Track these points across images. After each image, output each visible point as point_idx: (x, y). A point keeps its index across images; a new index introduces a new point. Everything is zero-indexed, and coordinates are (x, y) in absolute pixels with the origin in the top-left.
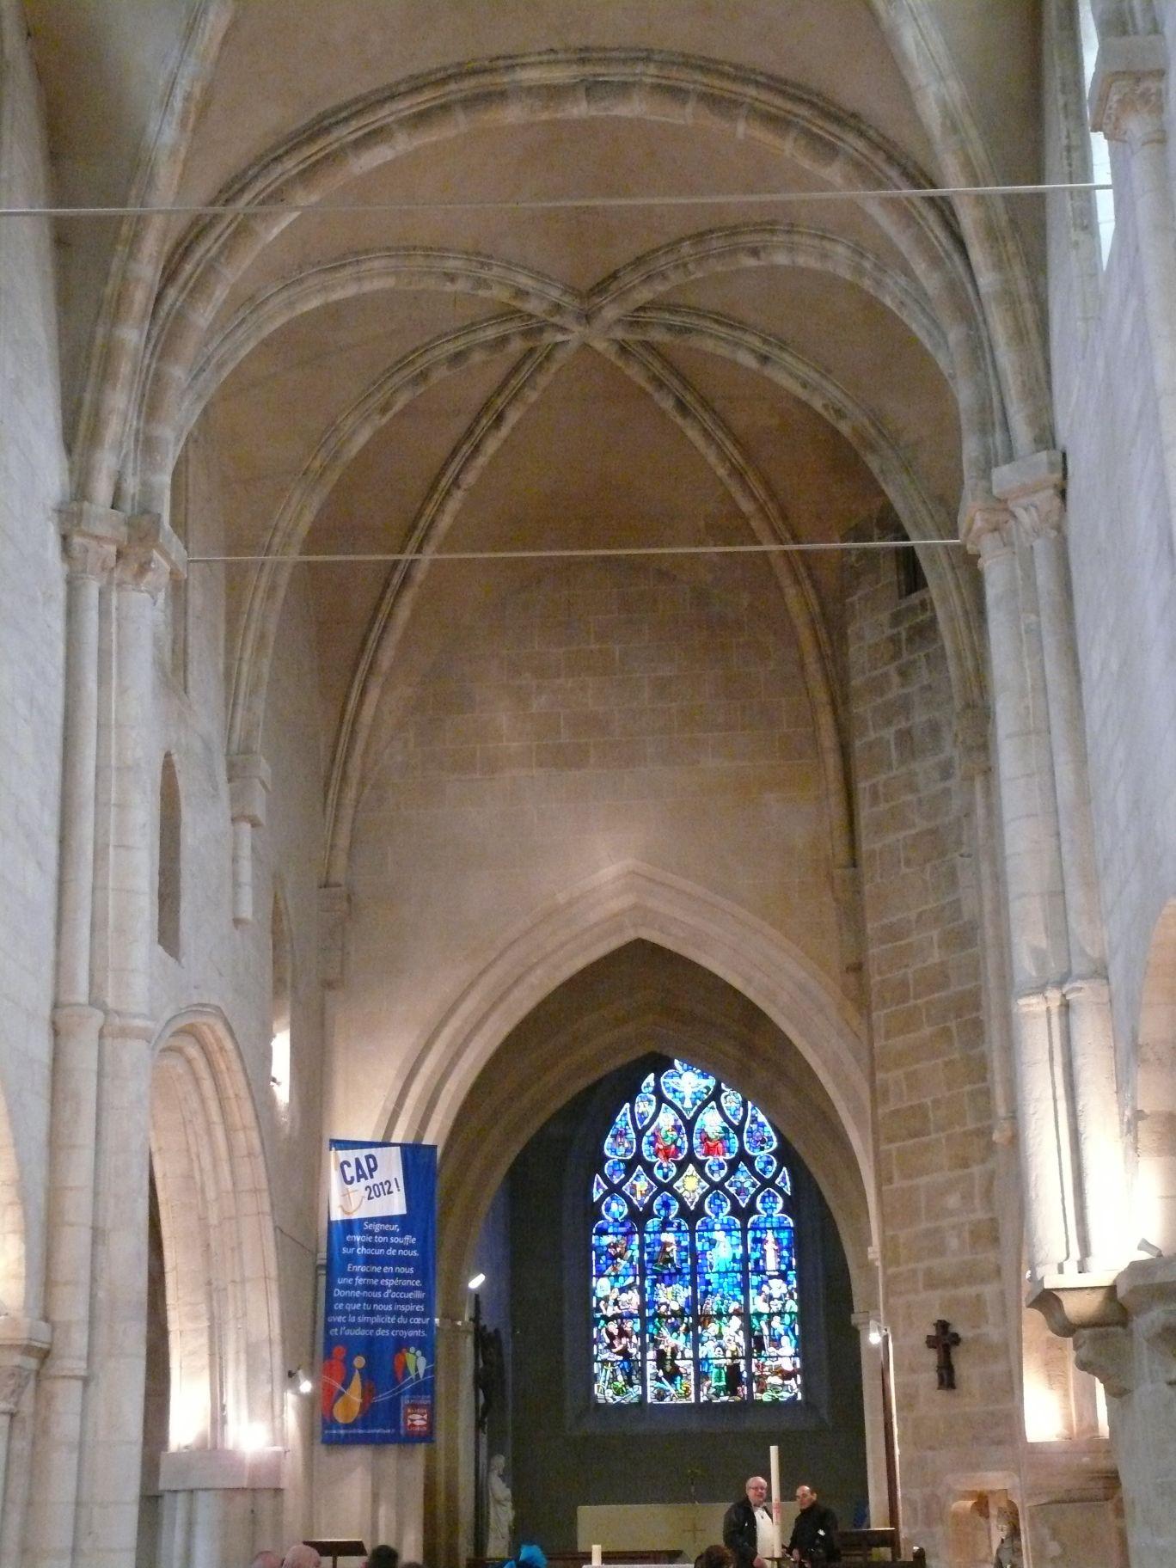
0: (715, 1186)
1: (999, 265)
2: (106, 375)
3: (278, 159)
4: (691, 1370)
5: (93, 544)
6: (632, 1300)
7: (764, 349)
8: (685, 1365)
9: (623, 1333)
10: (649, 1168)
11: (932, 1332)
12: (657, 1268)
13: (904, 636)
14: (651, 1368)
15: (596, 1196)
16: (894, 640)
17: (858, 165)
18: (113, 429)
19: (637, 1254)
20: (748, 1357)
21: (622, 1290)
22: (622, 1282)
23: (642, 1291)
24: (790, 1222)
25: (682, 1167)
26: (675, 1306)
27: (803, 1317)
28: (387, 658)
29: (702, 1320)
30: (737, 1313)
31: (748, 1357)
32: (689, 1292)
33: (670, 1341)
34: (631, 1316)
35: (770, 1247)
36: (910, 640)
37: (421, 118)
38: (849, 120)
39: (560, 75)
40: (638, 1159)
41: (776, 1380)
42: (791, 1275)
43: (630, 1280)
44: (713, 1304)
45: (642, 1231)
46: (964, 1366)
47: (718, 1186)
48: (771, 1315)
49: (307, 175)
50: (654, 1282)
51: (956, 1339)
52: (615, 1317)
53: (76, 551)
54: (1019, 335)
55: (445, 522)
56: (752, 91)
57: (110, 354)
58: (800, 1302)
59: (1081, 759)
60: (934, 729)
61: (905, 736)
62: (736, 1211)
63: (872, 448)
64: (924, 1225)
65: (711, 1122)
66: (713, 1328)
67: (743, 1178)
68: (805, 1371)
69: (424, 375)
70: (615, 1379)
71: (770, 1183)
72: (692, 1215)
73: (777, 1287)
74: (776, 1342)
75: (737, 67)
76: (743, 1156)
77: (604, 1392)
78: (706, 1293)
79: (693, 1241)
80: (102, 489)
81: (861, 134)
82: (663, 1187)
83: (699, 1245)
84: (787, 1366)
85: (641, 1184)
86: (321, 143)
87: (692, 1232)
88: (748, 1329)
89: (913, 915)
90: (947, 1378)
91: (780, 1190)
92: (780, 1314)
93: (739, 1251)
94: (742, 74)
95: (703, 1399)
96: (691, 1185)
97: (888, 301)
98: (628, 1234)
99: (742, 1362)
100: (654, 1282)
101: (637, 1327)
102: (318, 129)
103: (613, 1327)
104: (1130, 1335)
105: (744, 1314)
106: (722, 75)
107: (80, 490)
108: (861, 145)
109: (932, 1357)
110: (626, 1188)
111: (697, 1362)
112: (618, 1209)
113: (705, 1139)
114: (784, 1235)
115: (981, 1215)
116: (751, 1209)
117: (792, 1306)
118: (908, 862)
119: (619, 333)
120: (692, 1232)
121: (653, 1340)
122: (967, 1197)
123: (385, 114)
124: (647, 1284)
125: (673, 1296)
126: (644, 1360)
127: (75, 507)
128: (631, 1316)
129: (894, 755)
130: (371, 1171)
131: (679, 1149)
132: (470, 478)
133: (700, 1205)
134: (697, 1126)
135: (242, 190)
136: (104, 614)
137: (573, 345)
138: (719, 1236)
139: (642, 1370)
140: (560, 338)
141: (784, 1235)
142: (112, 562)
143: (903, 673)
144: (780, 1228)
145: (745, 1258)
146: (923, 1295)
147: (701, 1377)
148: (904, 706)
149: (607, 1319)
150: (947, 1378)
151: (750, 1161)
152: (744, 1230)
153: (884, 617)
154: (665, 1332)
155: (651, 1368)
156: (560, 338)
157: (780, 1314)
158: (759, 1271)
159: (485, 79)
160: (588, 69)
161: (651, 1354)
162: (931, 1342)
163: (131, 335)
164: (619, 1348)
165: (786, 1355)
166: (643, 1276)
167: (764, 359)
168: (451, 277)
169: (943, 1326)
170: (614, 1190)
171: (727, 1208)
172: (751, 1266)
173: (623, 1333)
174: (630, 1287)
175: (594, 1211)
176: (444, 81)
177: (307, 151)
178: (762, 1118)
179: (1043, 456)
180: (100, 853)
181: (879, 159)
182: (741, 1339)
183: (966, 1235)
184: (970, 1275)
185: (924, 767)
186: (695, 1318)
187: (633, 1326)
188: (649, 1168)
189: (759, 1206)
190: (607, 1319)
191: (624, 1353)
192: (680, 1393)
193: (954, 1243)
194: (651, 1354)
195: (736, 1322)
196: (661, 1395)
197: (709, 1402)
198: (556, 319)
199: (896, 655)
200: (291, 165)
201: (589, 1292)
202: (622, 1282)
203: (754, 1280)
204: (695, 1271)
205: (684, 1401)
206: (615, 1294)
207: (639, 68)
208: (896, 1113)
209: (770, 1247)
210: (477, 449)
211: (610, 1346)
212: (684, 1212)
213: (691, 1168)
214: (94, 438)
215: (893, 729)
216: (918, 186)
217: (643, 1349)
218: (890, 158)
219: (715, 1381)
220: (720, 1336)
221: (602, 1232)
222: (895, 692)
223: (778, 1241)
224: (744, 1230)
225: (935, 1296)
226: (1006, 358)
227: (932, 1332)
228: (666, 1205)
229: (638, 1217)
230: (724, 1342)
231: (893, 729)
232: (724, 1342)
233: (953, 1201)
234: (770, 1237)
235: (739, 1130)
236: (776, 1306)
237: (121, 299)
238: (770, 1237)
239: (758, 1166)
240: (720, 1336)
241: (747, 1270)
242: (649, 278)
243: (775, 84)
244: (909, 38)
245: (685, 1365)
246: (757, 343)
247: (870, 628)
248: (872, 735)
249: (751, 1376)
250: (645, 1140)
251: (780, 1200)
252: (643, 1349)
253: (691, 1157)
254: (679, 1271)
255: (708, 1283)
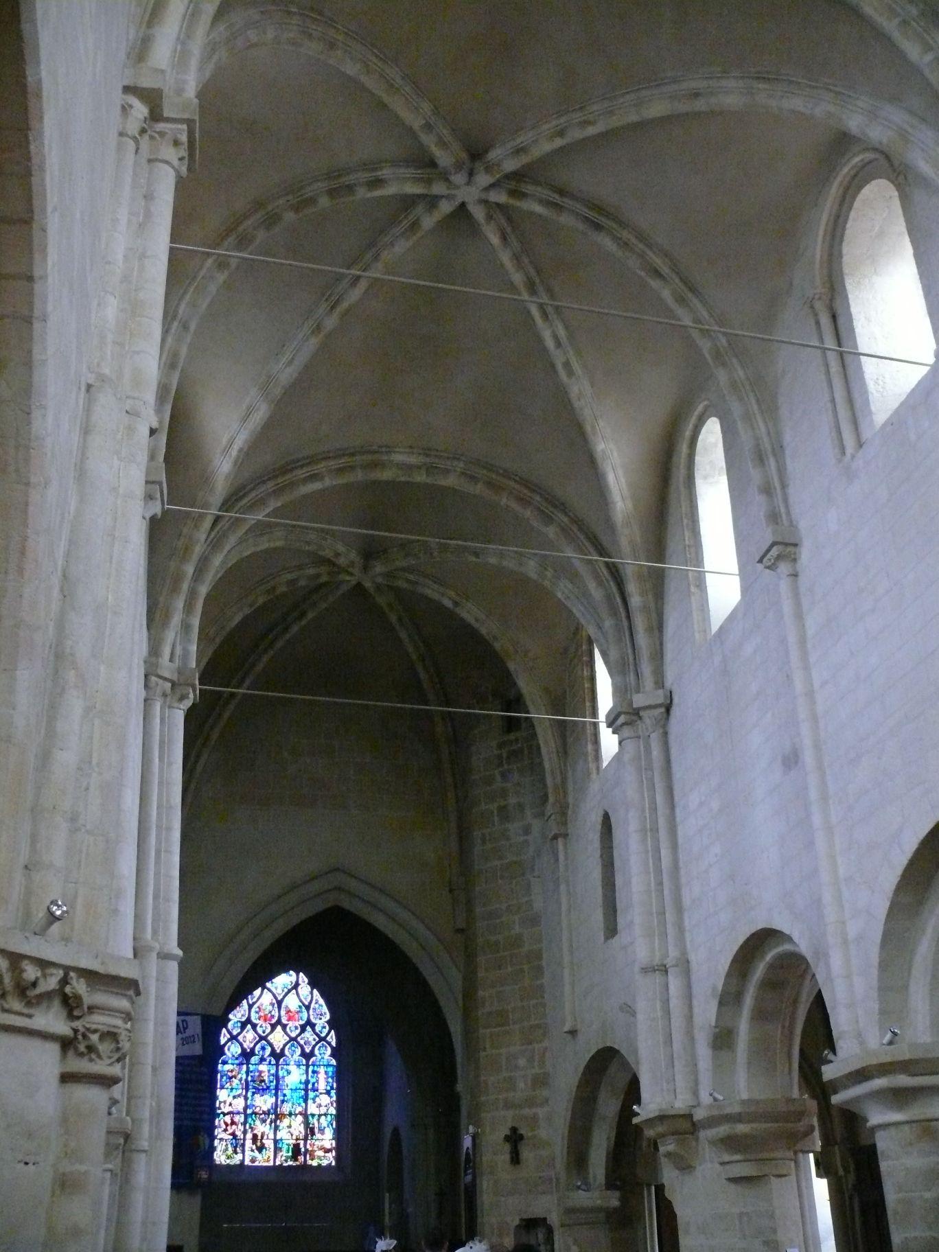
0: (292, 1039)
1: (643, 593)
2: (175, 589)
3: (264, 482)
4: (272, 1146)
5: (161, 681)
6: (239, 1104)
7: (458, 599)
8: (269, 1144)
9: (233, 1123)
10: (254, 1026)
11: (508, 1133)
12: (256, 1086)
13: (505, 755)
14: (249, 1143)
15: (223, 1041)
16: (500, 757)
17: (563, 529)
18: (176, 619)
19: (244, 1077)
20: (306, 1139)
21: (234, 1097)
22: (235, 1093)
23: (246, 1098)
24: (334, 1062)
25: (273, 1027)
26: (265, 1109)
27: (339, 1117)
28: (215, 735)
29: (279, 1116)
30: (300, 1113)
31: (306, 1139)
32: (273, 1100)
33: (260, 1128)
34: (238, 1113)
35: (322, 1076)
36: (508, 758)
37: (341, 470)
38: (563, 507)
39: (413, 460)
40: (249, 1021)
41: (321, 1153)
42: (333, 1092)
43: (239, 1092)
44: (286, 1108)
45: (248, 1064)
46: (526, 1153)
47: (295, 1039)
48: (320, 1116)
49: (278, 492)
50: (254, 1093)
51: (521, 1137)
52: (229, 1113)
53: (152, 684)
54: (650, 630)
55: (259, 667)
56: (512, 484)
57: (177, 579)
58: (338, 1109)
59: (674, 846)
60: (521, 807)
61: (502, 809)
62: (303, 1054)
63: (274, 588)
64: (505, 1074)
65: (292, 1002)
66: (286, 1122)
67: (309, 1035)
68: (338, 1148)
69: (274, 588)
70: (227, 1149)
71: (324, 1039)
72: (278, 1056)
73: (324, 1100)
74: (322, 1131)
75: (505, 471)
76: (309, 1023)
77: (220, 1157)
78: (283, 1102)
79: (277, 1071)
80: (167, 651)
81: (566, 514)
82: (261, 1038)
83: (281, 1073)
84: (328, 1146)
85: (249, 1037)
86: (288, 476)
87: (277, 1065)
88: (306, 1123)
89: (504, 906)
90: (516, 1159)
91: (329, 1044)
92: (325, 1115)
93: (304, 1078)
94: (507, 474)
95: (278, 1163)
96: (278, 1038)
97: (559, 595)
98: (240, 1064)
99: (302, 1143)
100: (254, 1093)
101: (242, 1120)
102: (285, 470)
103: (228, 1119)
104: (697, 1139)
105: (305, 1115)
106: (498, 474)
107: (154, 650)
108: (566, 520)
109: (507, 1147)
110: (240, 1038)
111: (276, 1142)
112: (233, 1050)
113: (288, 1011)
114: (330, 1069)
115: (537, 1070)
116: (312, 1054)
117: (333, 1111)
118: (502, 877)
119: (380, 580)
120: (277, 1065)
121: (251, 1128)
122: (531, 1060)
123: (321, 467)
124: (249, 1094)
125: (264, 1102)
126: (244, 1139)
127: (153, 659)
128: (238, 1113)
129: (496, 819)
130: (185, 1029)
131: (273, 1017)
132: (279, 644)
133: (283, 1050)
134: (283, 1005)
135: (244, 495)
136: (162, 720)
137: (354, 582)
138: (293, 1068)
139: (243, 1145)
140: (348, 578)
141: (330, 1069)
142: (169, 691)
143: (503, 775)
144: (328, 1065)
145: (307, 1082)
146: (502, 1113)
147: (277, 1150)
148: (504, 793)
149: (225, 1114)
150: (516, 1159)
151: (313, 1026)
152: (307, 1066)
153: (494, 744)
154: (258, 1122)
155: (249, 1143)
156: (348, 578)
157: (325, 1115)
158: (315, 1090)
159: (376, 456)
160: (428, 460)
161: (249, 1136)
162: (507, 1139)
163: (190, 569)
164: (230, 1131)
165: (327, 1139)
166: (247, 1090)
167: (456, 604)
168: (308, 543)
169: (514, 1130)
170: (233, 1038)
171: (299, 1051)
172: (310, 1086)
173: (233, 1123)
174: (239, 1096)
175: (220, 1051)
176: (353, 455)
177: (280, 480)
178: (321, 1001)
179: (661, 692)
180: (158, 852)
181: (575, 529)
182: (302, 1128)
183: (529, 1082)
184: (531, 1102)
185: (514, 827)
186: (276, 1115)
187: (239, 1119)
188: (254, 1026)
189: (316, 1052)
190: (225, 1114)
191: (233, 1134)
192: (265, 1159)
193: (522, 1085)
194: (249, 1136)
195: (300, 1118)
196: (253, 1160)
197: (281, 1165)
198: (350, 570)
199: (500, 765)
200: (270, 485)
201: (215, 1098)
202: (235, 1093)
203: (311, 1094)
204: (277, 1088)
205: (266, 1164)
206: (230, 1100)
207: (455, 463)
208: (490, 1013)
209: (322, 1076)
210: (286, 629)
211: (225, 1130)
212: (273, 1053)
213: (279, 1028)
214: (165, 623)
215: (496, 805)
216: (601, 555)
217: (245, 1132)
218: (580, 529)
219: (285, 1153)
220: (290, 1127)
221: (225, 1063)
222: (498, 783)
223: (326, 1073)
224: (307, 1066)
225: (510, 1114)
226: (642, 639)
227: (508, 1133)
228: (263, 1048)
229: (246, 1055)
230: (292, 1130)
231: (496, 805)
232: (292, 1130)
233: (522, 1062)
234: (322, 1070)
235: (308, 1008)
236: (323, 1110)
237: (187, 549)
238: (322, 1070)
239: (318, 1029)
240: (290, 1127)
241: (308, 1089)
242: (407, 555)
243: (525, 483)
244: (611, 478)
245: (269, 1144)
246: (452, 593)
247: (484, 750)
248: (483, 807)
249: (307, 1150)
250: (253, 1010)
251: (329, 1049)
252: (245, 1132)
253: (279, 1022)
254: (268, 1088)
255: (285, 1095)
